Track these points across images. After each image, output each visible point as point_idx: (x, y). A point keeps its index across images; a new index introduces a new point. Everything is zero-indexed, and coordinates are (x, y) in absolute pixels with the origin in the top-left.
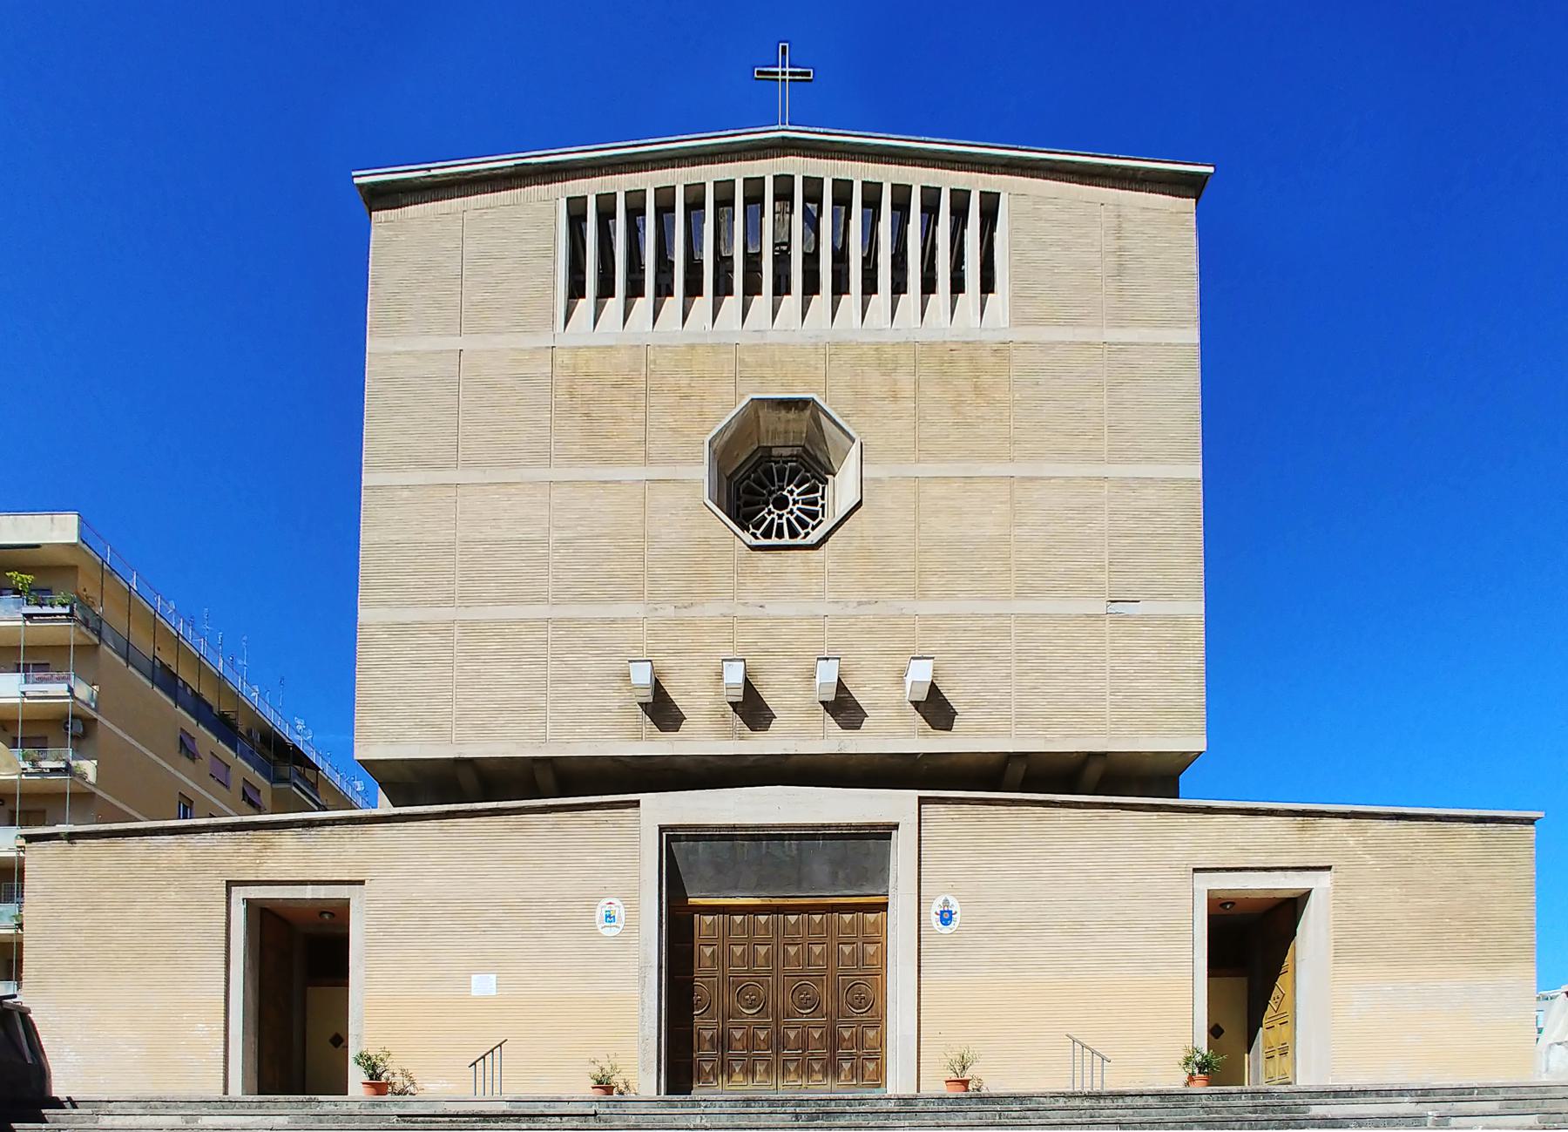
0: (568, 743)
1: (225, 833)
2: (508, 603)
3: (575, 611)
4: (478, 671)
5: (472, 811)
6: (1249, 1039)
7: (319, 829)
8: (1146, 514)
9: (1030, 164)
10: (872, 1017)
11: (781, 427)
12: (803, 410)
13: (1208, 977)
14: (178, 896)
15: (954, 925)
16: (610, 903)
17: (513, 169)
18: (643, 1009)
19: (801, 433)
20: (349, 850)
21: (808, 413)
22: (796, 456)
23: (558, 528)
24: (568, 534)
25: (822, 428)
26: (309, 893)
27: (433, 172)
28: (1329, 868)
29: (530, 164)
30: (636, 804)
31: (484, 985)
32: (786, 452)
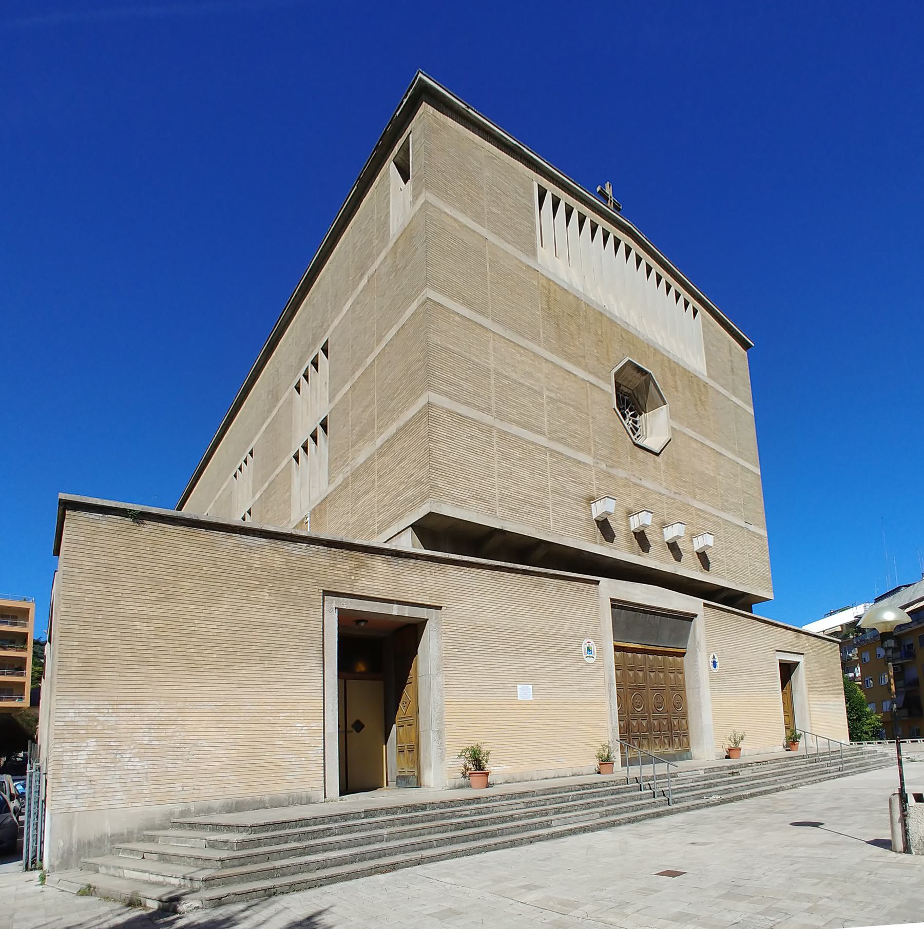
0: (563, 536)
1: (321, 547)
2: (524, 427)
5: (513, 569)
6: (385, 734)
7: (406, 560)
9: (609, 220)
10: (622, 714)
11: (630, 377)
12: (643, 375)
13: (338, 678)
14: (272, 598)
15: (718, 668)
16: (589, 642)
17: (512, 145)
18: (611, 710)
19: (636, 384)
20: (429, 581)
21: (644, 378)
22: (629, 394)
25: (649, 388)
26: (395, 610)
27: (470, 110)
28: (803, 654)
29: (523, 150)
30: (598, 582)
31: (525, 692)
32: (626, 390)
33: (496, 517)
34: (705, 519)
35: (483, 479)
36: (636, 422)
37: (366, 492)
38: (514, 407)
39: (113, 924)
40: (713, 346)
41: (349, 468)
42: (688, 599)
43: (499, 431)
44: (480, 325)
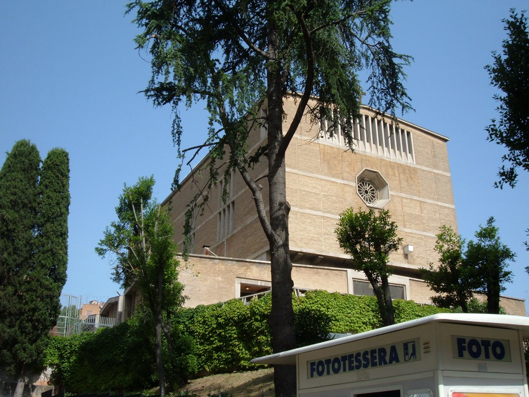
2: (312, 209)
3: (328, 215)
4: (305, 227)
8: (446, 215)
23: (323, 192)
24: (325, 194)
33: (299, 247)
34: (412, 237)
35: (293, 233)
36: (373, 193)
37: (250, 236)
38: (307, 202)
39: (316, 277)
40: (420, 147)
41: (243, 224)
42: (399, 277)
43: (300, 213)
44: (294, 173)
